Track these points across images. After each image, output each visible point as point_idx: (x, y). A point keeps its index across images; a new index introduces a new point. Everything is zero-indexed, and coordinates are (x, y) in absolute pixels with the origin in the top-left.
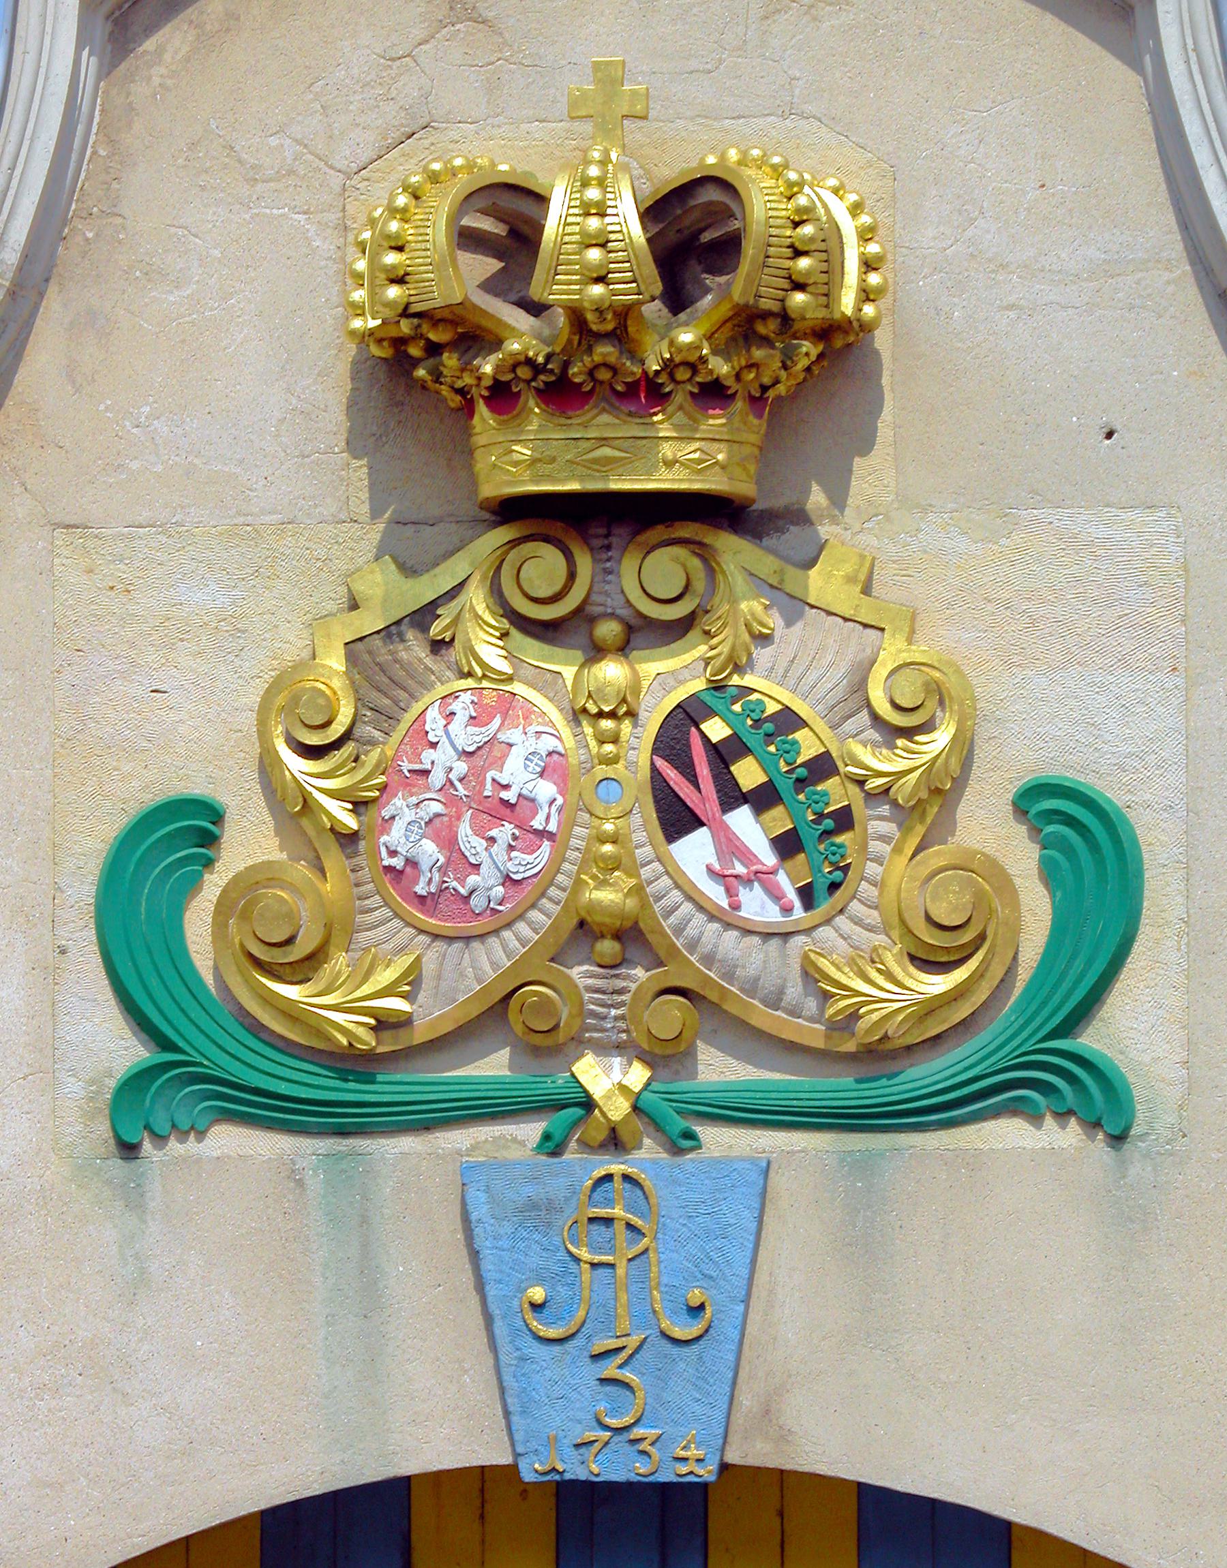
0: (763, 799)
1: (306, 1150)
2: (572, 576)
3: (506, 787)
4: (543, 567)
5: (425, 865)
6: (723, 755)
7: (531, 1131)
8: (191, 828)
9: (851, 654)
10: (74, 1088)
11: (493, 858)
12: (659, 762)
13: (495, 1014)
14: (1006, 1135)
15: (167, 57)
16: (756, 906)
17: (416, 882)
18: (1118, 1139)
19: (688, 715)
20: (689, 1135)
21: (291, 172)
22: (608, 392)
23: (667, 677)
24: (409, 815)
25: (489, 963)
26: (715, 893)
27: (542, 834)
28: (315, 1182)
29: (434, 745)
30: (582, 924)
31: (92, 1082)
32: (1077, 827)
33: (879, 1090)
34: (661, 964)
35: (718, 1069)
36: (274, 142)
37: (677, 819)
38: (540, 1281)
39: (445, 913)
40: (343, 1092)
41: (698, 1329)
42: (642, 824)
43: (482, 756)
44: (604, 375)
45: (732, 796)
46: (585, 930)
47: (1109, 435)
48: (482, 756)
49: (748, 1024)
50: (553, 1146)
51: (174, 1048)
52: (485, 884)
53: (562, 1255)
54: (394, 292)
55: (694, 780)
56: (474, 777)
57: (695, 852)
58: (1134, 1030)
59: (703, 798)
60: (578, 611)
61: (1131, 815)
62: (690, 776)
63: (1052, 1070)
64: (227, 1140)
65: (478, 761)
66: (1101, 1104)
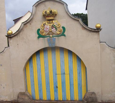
0: (55, 28)
6: (53, 26)
7: (49, 37)
11: (47, 30)
13: (48, 34)
14: (62, 37)
16: (55, 31)
19: (52, 25)
23: (52, 24)
32: (64, 28)
33: (58, 36)
35: (54, 35)
37: (52, 28)
39: (46, 32)
40: (44, 37)
41: (54, 43)
42: (51, 29)
43: (47, 27)
45: (54, 28)
46: (50, 32)
48: (47, 27)
50: (50, 38)
59: (53, 28)
62: (53, 27)
64: (41, 38)
66: (65, 36)
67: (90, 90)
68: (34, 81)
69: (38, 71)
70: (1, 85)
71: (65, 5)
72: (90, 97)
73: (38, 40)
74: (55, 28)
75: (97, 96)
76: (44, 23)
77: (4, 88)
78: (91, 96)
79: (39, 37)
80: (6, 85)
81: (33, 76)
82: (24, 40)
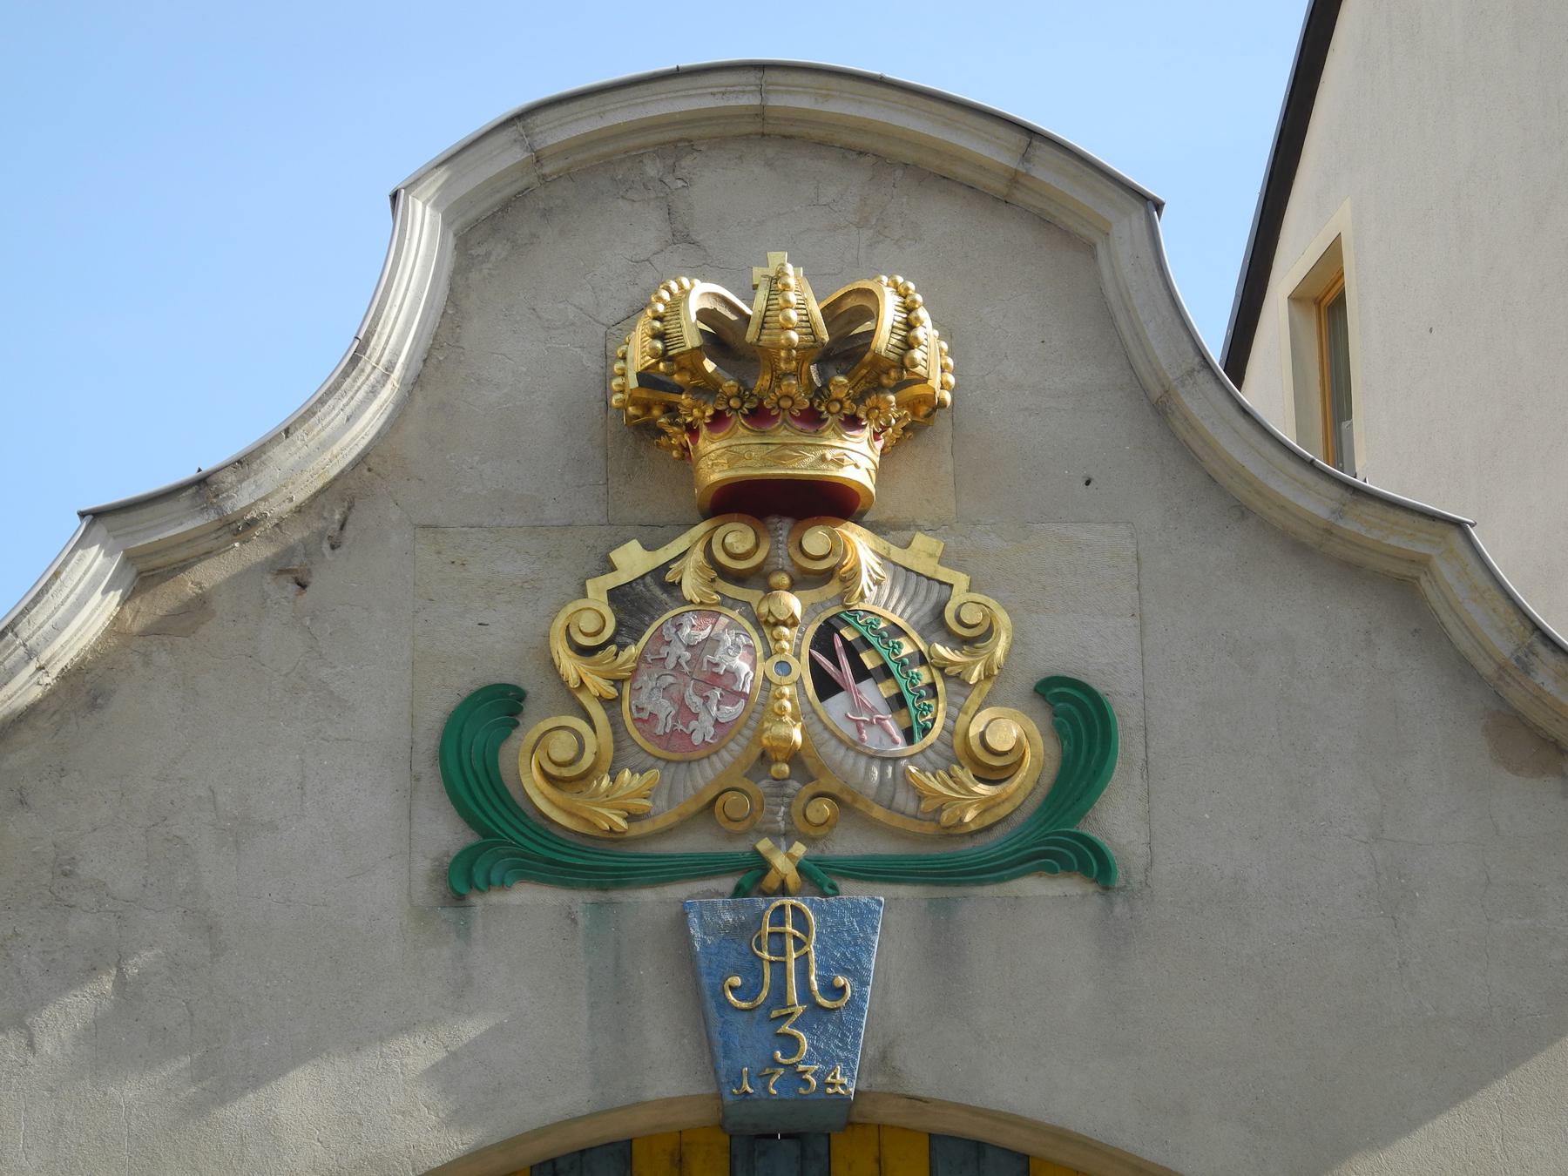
1: (579, 900)
2: (757, 546)
3: (717, 665)
4: (738, 537)
5: (662, 716)
6: (852, 651)
7: (727, 884)
8: (501, 706)
9: (934, 597)
10: (423, 866)
12: (814, 653)
14: (1032, 887)
15: (493, 258)
17: (655, 726)
18: (1107, 888)
20: (833, 887)
21: (573, 324)
22: (788, 418)
24: (652, 684)
25: (705, 778)
26: (849, 731)
27: (742, 695)
28: (583, 921)
29: (669, 643)
30: (763, 754)
31: (436, 859)
33: (947, 865)
34: (812, 779)
35: (848, 845)
36: (561, 306)
37: (826, 686)
38: (737, 973)
40: (594, 865)
44: (786, 404)
45: (861, 673)
47: (1088, 483)
49: (644, 1103)
50: (739, 892)
51: (494, 835)
52: (702, 730)
53: (749, 958)
54: (657, 324)
55: (837, 664)
56: (695, 661)
57: (838, 703)
58: (1115, 819)
60: (758, 569)
61: (1109, 699)
63: (1058, 840)
64: (527, 897)
65: (697, 651)
66: (1092, 863)
73: (465, 933)
74: (886, 689)
76: (633, 560)
79: (463, 880)
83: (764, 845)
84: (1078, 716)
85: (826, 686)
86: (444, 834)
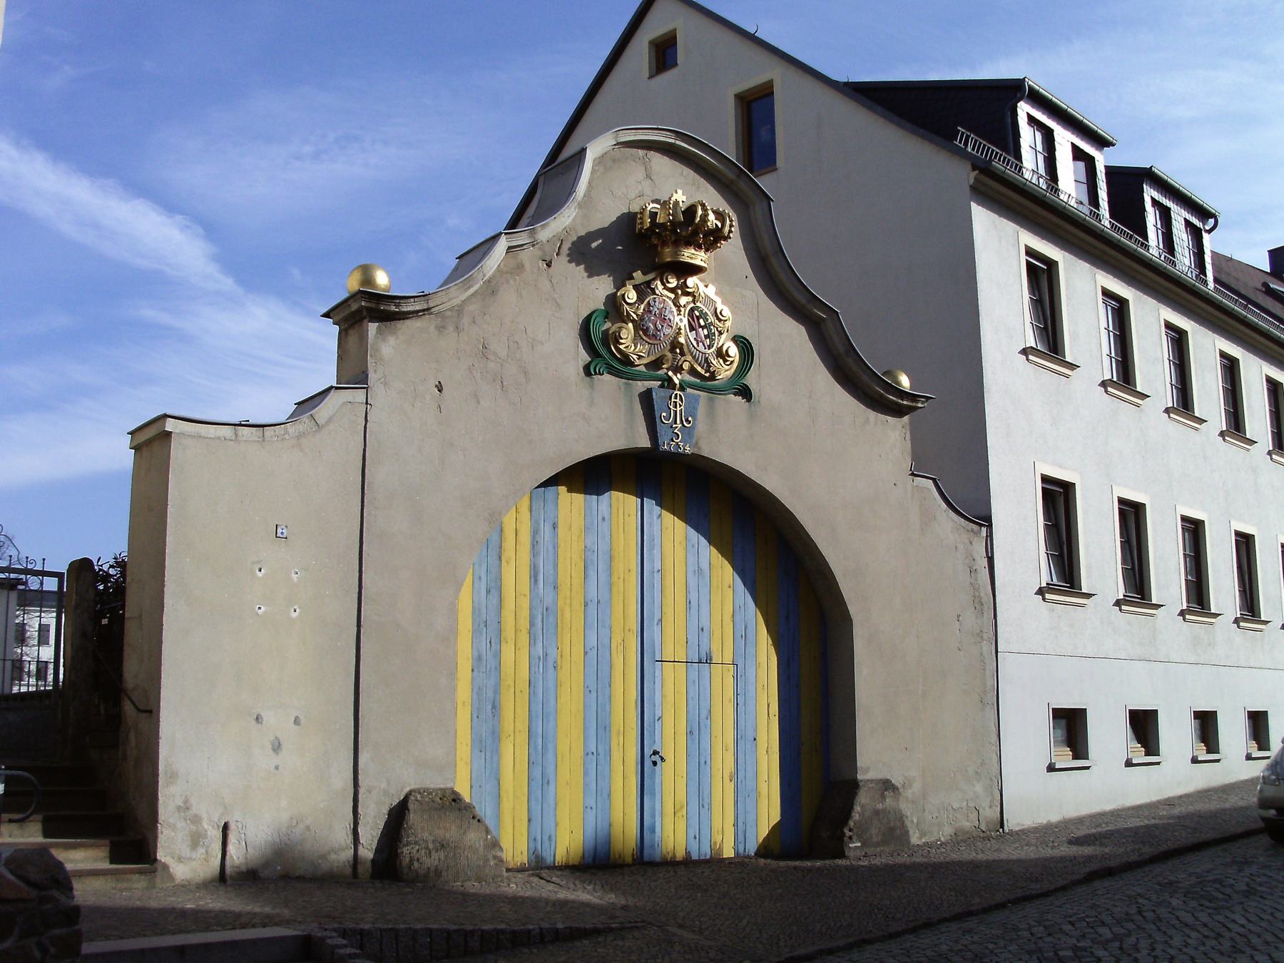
16: (701, 348)
50: (662, 386)
64: (607, 377)
66: (745, 393)
67: (867, 770)
68: (496, 707)
69: (532, 624)
70: (258, 719)
71: (170, 425)
72: (877, 812)
73: (592, 386)
75: (905, 807)
77: (277, 747)
78: (880, 806)
79: (587, 370)
80: (297, 721)
81: (498, 668)
82: (491, 365)
83: (670, 373)
84: (746, 347)
85: (692, 328)
86: (584, 357)
